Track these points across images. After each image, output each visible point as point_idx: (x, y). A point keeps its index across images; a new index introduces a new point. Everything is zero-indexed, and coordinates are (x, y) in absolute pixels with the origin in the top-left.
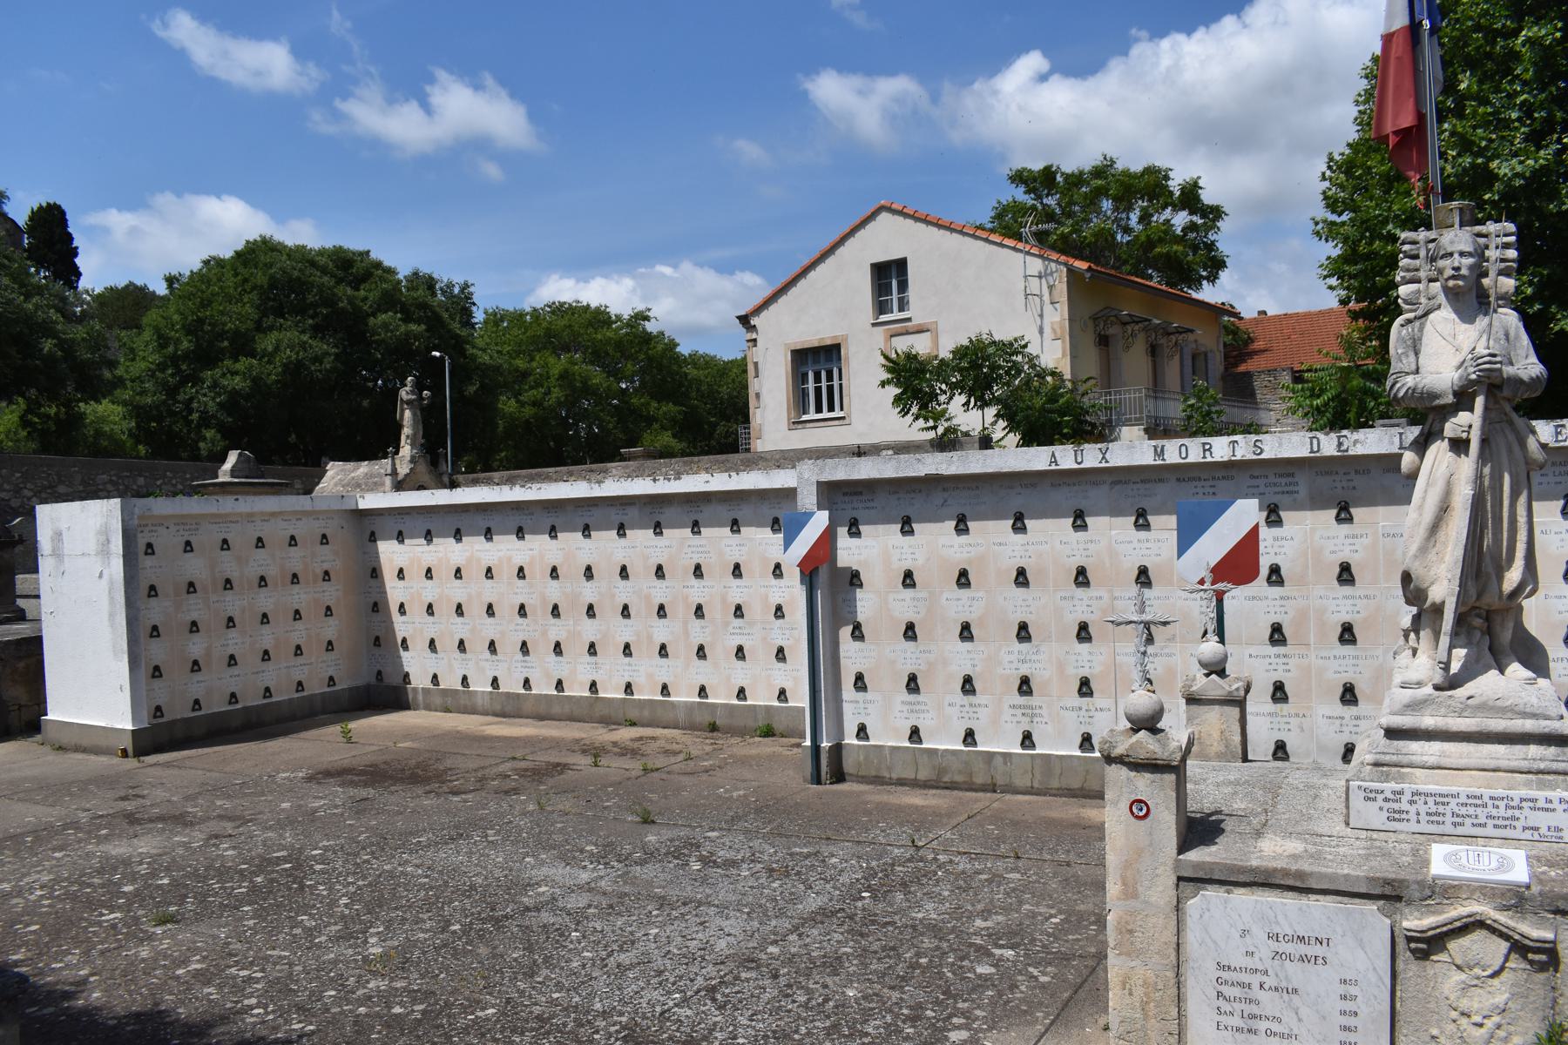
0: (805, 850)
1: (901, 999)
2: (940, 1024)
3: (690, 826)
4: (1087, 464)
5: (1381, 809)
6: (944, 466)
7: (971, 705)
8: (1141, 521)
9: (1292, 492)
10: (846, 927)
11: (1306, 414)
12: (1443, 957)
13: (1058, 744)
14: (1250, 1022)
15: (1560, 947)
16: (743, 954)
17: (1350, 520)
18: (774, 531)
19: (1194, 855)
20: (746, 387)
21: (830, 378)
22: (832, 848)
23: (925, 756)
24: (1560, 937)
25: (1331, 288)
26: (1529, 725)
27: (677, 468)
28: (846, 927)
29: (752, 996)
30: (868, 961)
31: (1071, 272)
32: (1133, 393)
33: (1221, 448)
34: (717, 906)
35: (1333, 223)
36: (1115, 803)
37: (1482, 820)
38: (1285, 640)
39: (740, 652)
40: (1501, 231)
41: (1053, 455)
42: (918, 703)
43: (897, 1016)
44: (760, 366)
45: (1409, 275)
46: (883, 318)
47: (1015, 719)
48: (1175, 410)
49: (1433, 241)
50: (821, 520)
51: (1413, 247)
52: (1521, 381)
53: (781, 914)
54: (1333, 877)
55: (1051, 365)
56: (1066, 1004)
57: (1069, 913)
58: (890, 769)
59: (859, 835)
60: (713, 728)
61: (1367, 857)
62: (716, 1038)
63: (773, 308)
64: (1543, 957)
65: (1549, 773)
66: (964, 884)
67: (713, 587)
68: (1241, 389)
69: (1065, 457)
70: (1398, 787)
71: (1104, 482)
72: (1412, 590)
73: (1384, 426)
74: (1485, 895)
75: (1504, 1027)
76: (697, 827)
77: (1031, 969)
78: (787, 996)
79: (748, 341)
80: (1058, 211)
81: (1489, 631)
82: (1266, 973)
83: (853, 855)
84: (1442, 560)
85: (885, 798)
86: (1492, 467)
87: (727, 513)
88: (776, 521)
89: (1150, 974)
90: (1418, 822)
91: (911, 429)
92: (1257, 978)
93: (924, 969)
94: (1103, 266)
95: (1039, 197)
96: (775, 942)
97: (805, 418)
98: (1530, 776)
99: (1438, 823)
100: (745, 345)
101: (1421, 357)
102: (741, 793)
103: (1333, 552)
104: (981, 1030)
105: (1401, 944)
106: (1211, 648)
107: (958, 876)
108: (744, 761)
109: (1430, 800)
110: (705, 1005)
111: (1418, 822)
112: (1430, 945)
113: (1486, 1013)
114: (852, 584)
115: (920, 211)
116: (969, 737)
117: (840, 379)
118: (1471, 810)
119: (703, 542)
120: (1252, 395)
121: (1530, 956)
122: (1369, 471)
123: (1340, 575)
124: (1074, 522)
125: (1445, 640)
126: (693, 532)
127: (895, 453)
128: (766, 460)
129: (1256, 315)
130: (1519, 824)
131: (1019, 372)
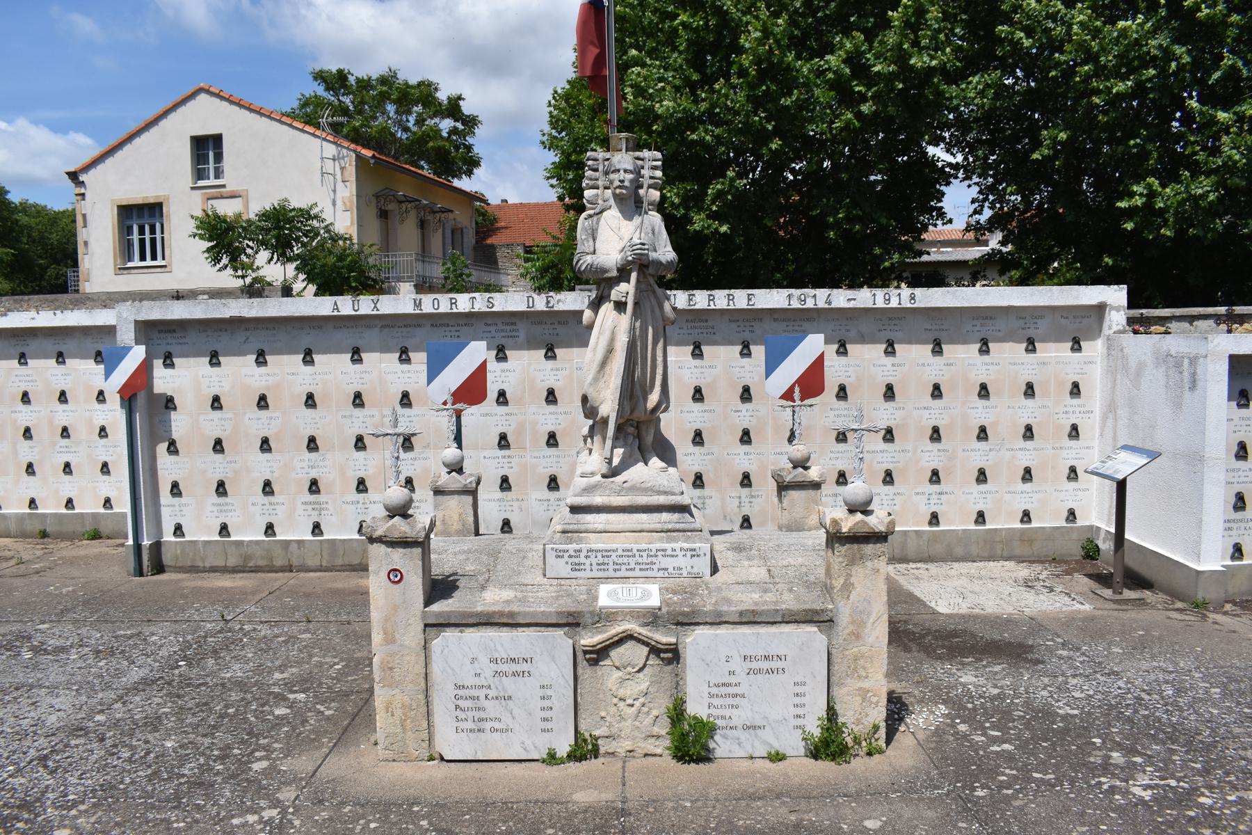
0: (129, 632)
1: (212, 743)
2: (246, 758)
3: (21, 621)
4: (362, 311)
5: (567, 563)
6: (246, 310)
7: (270, 504)
8: (404, 357)
10: (165, 691)
13: (341, 530)
14: (479, 724)
15: (680, 647)
16: (73, 725)
17: (554, 357)
18: (97, 362)
19: (436, 607)
20: (75, 235)
21: (153, 231)
22: (153, 629)
23: (233, 547)
24: (680, 641)
25: (552, 186)
27: (7, 305)
28: (165, 691)
29: (81, 758)
30: (184, 717)
31: (359, 158)
32: (406, 256)
33: (464, 302)
34: (48, 688)
35: (555, 138)
36: (377, 573)
37: (632, 566)
39: (67, 468)
40: (652, 157)
41: (336, 303)
42: (227, 504)
43: (209, 757)
44: (88, 217)
45: (591, 183)
46: (201, 183)
47: (306, 513)
48: (437, 271)
49: (608, 159)
50: (138, 354)
53: (107, 687)
54: (534, 614)
55: (342, 231)
56: (346, 730)
57: (349, 661)
58: (203, 560)
59: (176, 615)
60: (44, 534)
61: (557, 598)
62: (48, 798)
63: (100, 167)
64: (670, 655)
66: (266, 645)
67: (39, 412)
68: (486, 257)
69: (345, 305)
70: (577, 547)
71: (376, 326)
72: (589, 408)
73: (581, 290)
76: (28, 622)
77: (318, 707)
78: (113, 754)
79: (77, 195)
80: (351, 108)
81: (639, 436)
82: (489, 687)
83: (171, 632)
85: (199, 583)
87: (51, 346)
88: (99, 354)
89: (406, 699)
91: (227, 279)
92: (485, 691)
93: (232, 717)
94: (385, 155)
95: (336, 95)
96: (102, 711)
97: (130, 265)
100: (74, 199)
101: (597, 242)
102: (70, 589)
103: (543, 381)
104: (279, 759)
106: (451, 452)
107: (260, 641)
108: (72, 562)
109: (599, 554)
110: (37, 772)
112: (598, 655)
114: (167, 407)
115: (235, 95)
116: (270, 529)
117: (162, 233)
118: (625, 560)
119: (30, 372)
120: (495, 262)
121: (662, 655)
122: (568, 323)
124: (352, 357)
125: (609, 443)
126: (20, 363)
127: (210, 298)
128: (93, 300)
129: (500, 202)
131: (317, 234)
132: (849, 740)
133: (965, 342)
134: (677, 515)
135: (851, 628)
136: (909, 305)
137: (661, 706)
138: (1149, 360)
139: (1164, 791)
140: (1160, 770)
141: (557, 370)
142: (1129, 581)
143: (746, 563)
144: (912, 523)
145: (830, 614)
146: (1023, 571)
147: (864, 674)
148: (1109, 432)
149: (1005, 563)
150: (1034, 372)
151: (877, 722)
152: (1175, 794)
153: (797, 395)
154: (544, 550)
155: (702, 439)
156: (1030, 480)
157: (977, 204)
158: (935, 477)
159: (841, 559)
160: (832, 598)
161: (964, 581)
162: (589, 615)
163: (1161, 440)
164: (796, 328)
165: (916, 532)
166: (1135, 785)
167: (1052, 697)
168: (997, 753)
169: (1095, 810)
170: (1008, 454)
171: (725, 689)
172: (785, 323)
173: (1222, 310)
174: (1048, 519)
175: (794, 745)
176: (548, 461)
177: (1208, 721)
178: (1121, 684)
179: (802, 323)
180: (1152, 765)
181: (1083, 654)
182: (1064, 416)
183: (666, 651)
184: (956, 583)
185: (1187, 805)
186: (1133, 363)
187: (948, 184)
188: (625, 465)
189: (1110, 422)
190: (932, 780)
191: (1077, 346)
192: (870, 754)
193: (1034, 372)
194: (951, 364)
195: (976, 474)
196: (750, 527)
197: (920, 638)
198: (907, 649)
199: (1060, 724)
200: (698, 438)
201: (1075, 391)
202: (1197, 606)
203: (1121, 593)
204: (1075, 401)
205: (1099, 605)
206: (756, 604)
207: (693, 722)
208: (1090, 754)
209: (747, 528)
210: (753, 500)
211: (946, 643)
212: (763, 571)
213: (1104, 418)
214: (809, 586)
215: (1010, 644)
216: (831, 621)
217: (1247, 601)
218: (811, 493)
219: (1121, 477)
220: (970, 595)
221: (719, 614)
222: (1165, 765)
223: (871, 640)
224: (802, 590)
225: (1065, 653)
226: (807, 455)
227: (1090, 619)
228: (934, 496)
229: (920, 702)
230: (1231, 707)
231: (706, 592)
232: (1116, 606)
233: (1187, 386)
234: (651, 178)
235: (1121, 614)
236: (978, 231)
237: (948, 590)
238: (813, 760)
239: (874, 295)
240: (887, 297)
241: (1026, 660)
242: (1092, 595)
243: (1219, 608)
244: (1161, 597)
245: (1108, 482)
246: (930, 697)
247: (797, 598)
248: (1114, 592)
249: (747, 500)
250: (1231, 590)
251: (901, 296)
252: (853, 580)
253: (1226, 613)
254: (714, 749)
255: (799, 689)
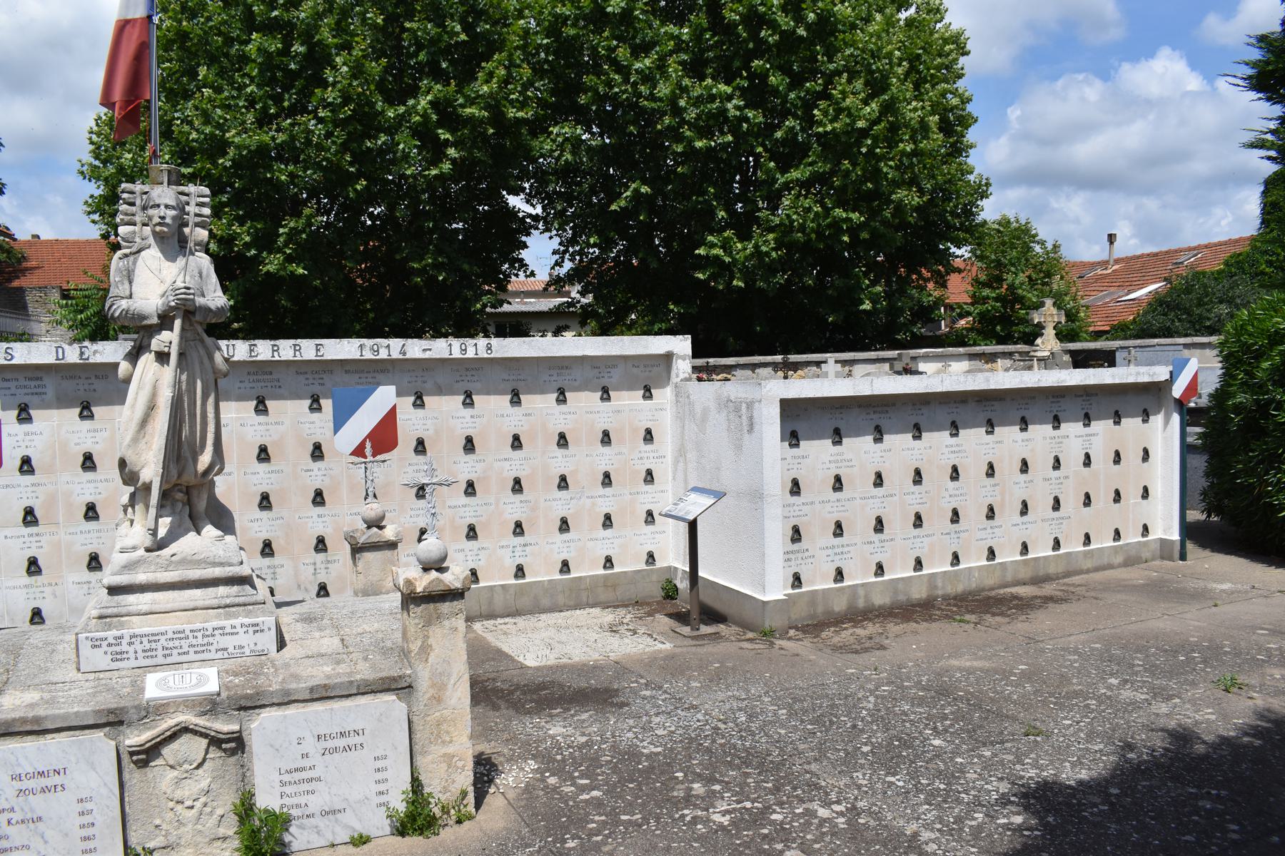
5: (106, 653)
9: (40, 394)
11: (71, 327)
12: (159, 762)
15: (244, 734)
17: (91, 417)
24: (244, 727)
25: (93, 222)
26: (217, 572)
37: (185, 649)
38: (37, 521)
45: (127, 218)
49: (146, 193)
51: (131, 196)
52: (209, 310)
54: (65, 717)
61: (94, 695)
64: (233, 745)
65: (233, 606)
68: (16, 304)
70: (118, 633)
72: (128, 474)
73: (126, 340)
74: (187, 707)
75: (209, 804)
81: (189, 503)
82: (12, 810)
84: (150, 448)
86: (188, 375)
90: (136, 658)
98: (220, 610)
99: (152, 657)
105: (126, 759)
109: (145, 640)
111: (136, 658)
112: (148, 755)
113: (195, 797)
118: (177, 643)
120: (25, 307)
121: (224, 746)
122: (107, 377)
123: (84, 463)
125: (153, 511)
129: (29, 238)
130: (213, 648)
132: (437, 811)
133: (543, 392)
134: (235, 588)
135: (431, 692)
136: (486, 356)
137: (226, 802)
138: (712, 405)
139: (741, 814)
140: (736, 794)
141: (95, 431)
142: (705, 617)
143: (317, 634)
144: (496, 577)
145: (409, 680)
146: (608, 617)
147: (448, 739)
148: (680, 475)
149: (591, 610)
150: (610, 420)
151: (464, 788)
152: (750, 815)
153: (368, 450)
154: (77, 640)
155: (269, 503)
156: (611, 526)
157: (557, 256)
158: (519, 529)
159: (417, 621)
160: (409, 663)
161: (552, 632)
162: (133, 711)
163: (727, 480)
164: (371, 380)
165: (502, 586)
166: (715, 813)
167: (637, 737)
168: (586, 801)
169: (679, 843)
170: (589, 501)
171: (301, 775)
172: (357, 376)
173: (779, 358)
174: (629, 564)
175: (378, 824)
176: (87, 538)
177: (777, 742)
178: (700, 716)
179: (376, 375)
180: (729, 790)
181: (665, 692)
182: (640, 462)
183: (228, 741)
184: (544, 634)
185: (761, 824)
186: (698, 409)
187: (528, 234)
188: (173, 536)
189: (681, 465)
190: (523, 839)
191: (648, 394)
192: (459, 822)
193: (610, 420)
194: (530, 415)
195: (559, 523)
196: (327, 594)
197: (508, 695)
198: (496, 708)
199: (645, 764)
200: (265, 502)
201: (648, 437)
202: (765, 635)
203: (698, 629)
204: (649, 447)
205: (679, 643)
206: (328, 677)
207: (264, 817)
208: (673, 789)
209: (323, 596)
210: (329, 565)
211: (535, 697)
212: (336, 641)
213: (676, 462)
214: (385, 652)
215: (596, 690)
216: (410, 687)
217: (808, 625)
218: (387, 553)
219: (691, 518)
220: (557, 645)
221: (287, 693)
222: (741, 789)
223: (453, 701)
224: (378, 657)
225: (648, 693)
226: (381, 514)
227: (670, 657)
228: (519, 548)
229: (510, 760)
230: (796, 726)
231: (272, 670)
232: (694, 642)
233: (746, 429)
234: (197, 215)
235: (699, 650)
236: (557, 284)
237: (536, 642)
238: (400, 838)
239: (450, 345)
240: (463, 347)
241: (612, 705)
242: (672, 634)
243: (784, 635)
244: (734, 629)
245: (682, 524)
246: (519, 753)
247: (373, 667)
248: (692, 629)
249: (323, 566)
250: (793, 617)
251: (477, 347)
252: (430, 641)
253: (790, 639)
254: (290, 842)
255: (380, 764)
